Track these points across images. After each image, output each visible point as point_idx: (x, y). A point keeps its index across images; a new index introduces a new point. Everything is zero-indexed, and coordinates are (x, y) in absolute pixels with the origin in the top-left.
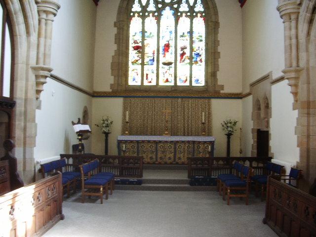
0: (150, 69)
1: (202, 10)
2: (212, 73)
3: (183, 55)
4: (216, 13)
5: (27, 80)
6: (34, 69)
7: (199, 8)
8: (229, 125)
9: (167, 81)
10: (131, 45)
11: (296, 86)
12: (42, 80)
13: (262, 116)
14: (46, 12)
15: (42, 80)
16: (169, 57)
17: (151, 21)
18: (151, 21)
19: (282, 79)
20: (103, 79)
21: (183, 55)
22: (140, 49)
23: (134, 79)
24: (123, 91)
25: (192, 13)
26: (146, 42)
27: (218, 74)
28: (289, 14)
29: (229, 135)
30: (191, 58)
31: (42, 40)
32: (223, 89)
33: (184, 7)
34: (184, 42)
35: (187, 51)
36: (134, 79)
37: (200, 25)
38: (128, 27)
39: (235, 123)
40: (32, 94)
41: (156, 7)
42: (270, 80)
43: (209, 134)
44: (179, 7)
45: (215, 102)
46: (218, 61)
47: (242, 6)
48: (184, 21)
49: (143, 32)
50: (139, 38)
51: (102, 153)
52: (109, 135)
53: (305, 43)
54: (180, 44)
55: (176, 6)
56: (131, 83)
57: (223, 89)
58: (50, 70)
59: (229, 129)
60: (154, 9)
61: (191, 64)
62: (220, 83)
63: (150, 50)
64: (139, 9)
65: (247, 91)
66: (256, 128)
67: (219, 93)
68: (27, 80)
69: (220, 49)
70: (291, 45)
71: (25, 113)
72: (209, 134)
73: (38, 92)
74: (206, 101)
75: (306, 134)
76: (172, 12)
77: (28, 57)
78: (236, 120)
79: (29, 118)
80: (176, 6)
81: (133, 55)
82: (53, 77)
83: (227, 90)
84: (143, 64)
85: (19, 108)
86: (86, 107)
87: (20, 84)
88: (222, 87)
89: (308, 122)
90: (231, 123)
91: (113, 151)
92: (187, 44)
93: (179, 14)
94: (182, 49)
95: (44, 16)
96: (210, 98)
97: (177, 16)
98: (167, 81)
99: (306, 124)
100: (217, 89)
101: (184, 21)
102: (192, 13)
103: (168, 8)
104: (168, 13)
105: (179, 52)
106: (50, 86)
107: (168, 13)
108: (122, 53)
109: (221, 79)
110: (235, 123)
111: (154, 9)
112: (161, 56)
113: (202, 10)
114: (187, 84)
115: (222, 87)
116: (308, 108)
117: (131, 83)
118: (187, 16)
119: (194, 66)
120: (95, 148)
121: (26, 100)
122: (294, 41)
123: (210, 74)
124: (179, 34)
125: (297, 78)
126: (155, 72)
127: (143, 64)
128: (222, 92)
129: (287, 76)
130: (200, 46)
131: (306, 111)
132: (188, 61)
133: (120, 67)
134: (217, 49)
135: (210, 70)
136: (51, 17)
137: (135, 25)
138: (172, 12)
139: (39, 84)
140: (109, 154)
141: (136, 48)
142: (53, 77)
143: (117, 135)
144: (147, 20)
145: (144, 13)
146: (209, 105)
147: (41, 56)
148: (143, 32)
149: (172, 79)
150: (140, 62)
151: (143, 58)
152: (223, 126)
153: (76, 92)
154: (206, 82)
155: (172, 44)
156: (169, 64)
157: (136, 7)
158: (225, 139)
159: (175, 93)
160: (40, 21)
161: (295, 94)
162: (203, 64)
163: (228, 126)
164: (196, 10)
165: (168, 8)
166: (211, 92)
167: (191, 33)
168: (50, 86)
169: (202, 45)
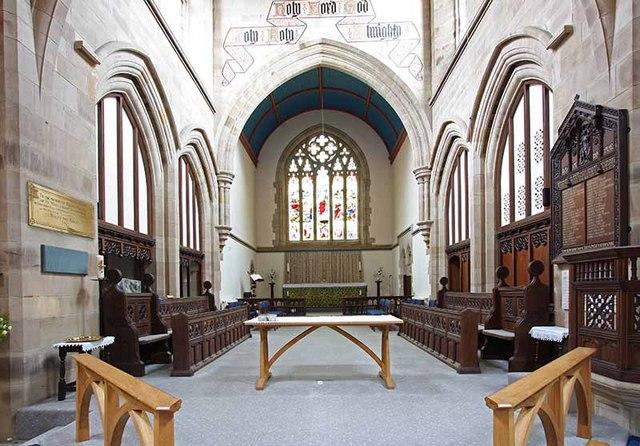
0: (308, 226)
1: (355, 168)
2: (364, 228)
3: (337, 212)
4: (368, 173)
5: (213, 238)
6: (218, 228)
7: (352, 166)
9: (324, 235)
10: (290, 204)
11: (428, 235)
12: (224, 237)
13: (407, 263)
14: (225, 182)
15: (224, 237)
16: (326, 216)
17: (307, 182)
18: (307, 182)
19: (417, 231)
20: (269, 235)
21: (337, 212)
22: (299, 207)
23: (294, 236)
24: (283, 246)
25: (345, 173)
26: (303, 201)
28: (422, 177)
29: (378, 283)
30: (345, 214)
31: (222, 205)
33: (338, 166)
34: (338, 200)
35: (342, 208)
36: (294, 236)
37: (352, 183)
38: (287, 187)
40: (217, 248)
41: (312, 167)
42: (411, 232)
43: (361, 279)
44: (333, 165)
47: (391, 163)
48: (338, 182)
49: (301, 191)
50: (296, 197)
54: (334, 203)
55: (330, 165)
56: (291, 239)
58: (230, 229)
60: (310, 170)
61: (345, 220)
63: (307, 207)
64: (296, 170)
65: (396, 242)
68: (213, 238)
71: (213, 263)
72: (361, 279)
73: (222, 247)
74: (357, 252)
76: (327, 171)
77: (212, 219)
79: (215, 267)
80: (330, 165)
81: (292, 213)
82: (231, 236)
83: (377, 243)
84: (301, 222)
85: (207, 260)
86: (252, 262)
87: (207, 241)
91: (278, 295)
92: (341, 202)
93: (341, 145)
94: (337, 206)
95: (222, 185)
97: (331, 175)
98: (324, 235)
101: (338, 182)
102: (345, 173)
103: (323, 168)
104: (323, 173)
105: (334, 209)
106: (229, 242)
107: (323, 173)
108: (282, 213)
111: (310, 170)
112: (318, 213)
113: (355, 168)
114: (342, 238)
117: (291, 239)
118: (340, 175)
119: (348, 221)
120: (262, 293)
121: (212, 253)
122: (426, 199)
124: (334, 192)
126: (312, 227)
127: (301, 222)
129: (421, 227)
130: (353, 203)
132: (342, 217)
133: (281, 224)
136: (228, 185)
137: (293, 186)
138: (327, 171)
139: (221, 240)
141: (294, 207)
142: (231, 236)
143: (281, 285)
144: (304, 180)
145: (300, 174)
147: (222, 217)
148: (301, 191)
149: (328, 234)
150: (298, 219)
151: (301, 216)
153: (251, 250)
154: (359, 235)
155: (328, 202)
156: (325, 222)
157: (293, 168)
159: (332, 247)
160: (219, 188)
161: (428, 242)
162: (356, 219)
164: (349, 168)
165: (323, 168)
166: (364, 244)
167: (345, 191)
168: (229, 242)
169: (355, 201)
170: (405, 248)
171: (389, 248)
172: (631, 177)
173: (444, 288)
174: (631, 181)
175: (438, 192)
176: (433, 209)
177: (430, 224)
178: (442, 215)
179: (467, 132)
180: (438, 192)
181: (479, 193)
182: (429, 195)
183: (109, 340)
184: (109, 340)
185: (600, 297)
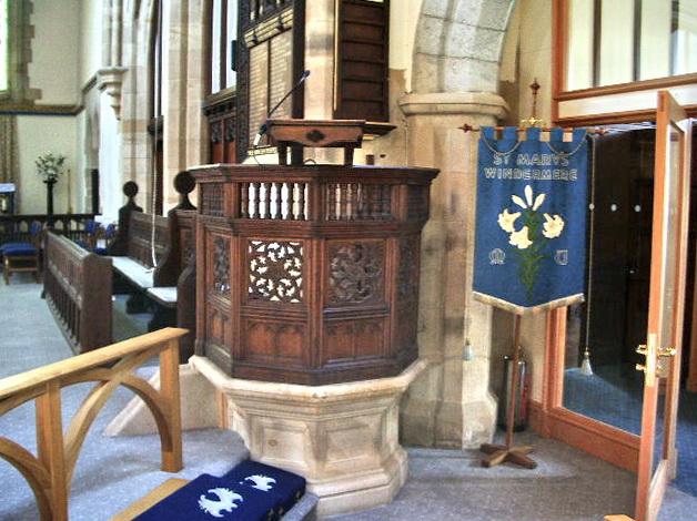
8: (50, 164)
27: (30, 66)
29: (51, 183)
32: (40, 98)
39: (61, 161)
42: (98, 85)
45: (23, 122)
46: (29, 42)
51: (44, 211)
52: (54, 185)
53: (130, 30)
57: (40, 98)
59: (50, 171)
62: (33, 85)
66: (91, 167)
67: (31, 103)
69: (33, 21)
70: (110, 30)
74: (8, 119)
75: (129, 171)
78: (63, 154)
83: (48, 99)
88: (38, 93)
89: (133, 152)
90: (52, 160)
96: (13, 114)
99: (129, 155)
100: (29, 97)
109: (37, 75)
110: (61, 161)
115: (38, 93)
116: (134, 130)
122: (115, 24)
123: (15, 68)
125: (118, 84)
128: (37, 102)
131: (129, 136)
134: (28, 20)
135: (15, 61)
140: (56, 211)
146: (13, 127)
152: (39, 166)
154: (10, 82)
158: (44, 188)
161: (117, 109)
163: (47, 167)
170: (93, 117)
171: (70, 111)
172: (308, 44)
173: (185, 204)
174: (307, 52)
175: (137, 14)
176: (128, 47)
177: (119, 73)
178: (143, 60)
179: (522, 334)
180: (137, 14)
181: (178, 29)
182: (120, 18)
183: (546, 215)
184: (546, 215)
185: (553, 227)
